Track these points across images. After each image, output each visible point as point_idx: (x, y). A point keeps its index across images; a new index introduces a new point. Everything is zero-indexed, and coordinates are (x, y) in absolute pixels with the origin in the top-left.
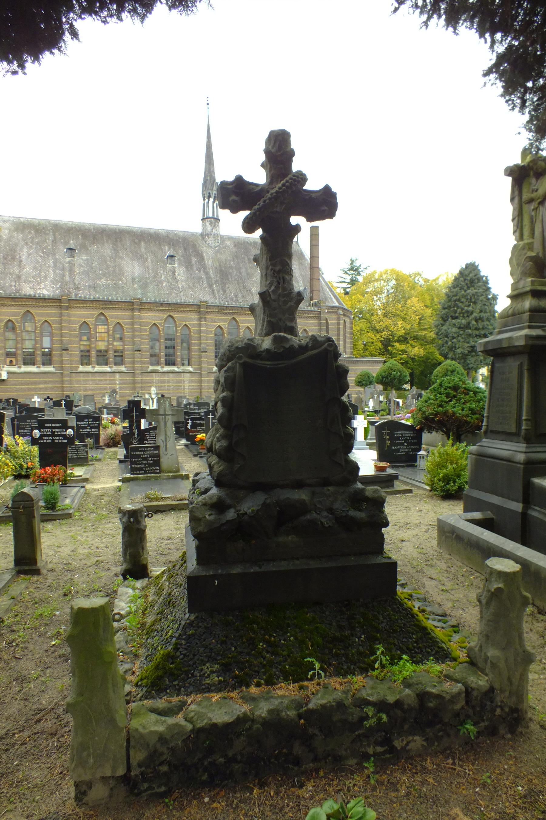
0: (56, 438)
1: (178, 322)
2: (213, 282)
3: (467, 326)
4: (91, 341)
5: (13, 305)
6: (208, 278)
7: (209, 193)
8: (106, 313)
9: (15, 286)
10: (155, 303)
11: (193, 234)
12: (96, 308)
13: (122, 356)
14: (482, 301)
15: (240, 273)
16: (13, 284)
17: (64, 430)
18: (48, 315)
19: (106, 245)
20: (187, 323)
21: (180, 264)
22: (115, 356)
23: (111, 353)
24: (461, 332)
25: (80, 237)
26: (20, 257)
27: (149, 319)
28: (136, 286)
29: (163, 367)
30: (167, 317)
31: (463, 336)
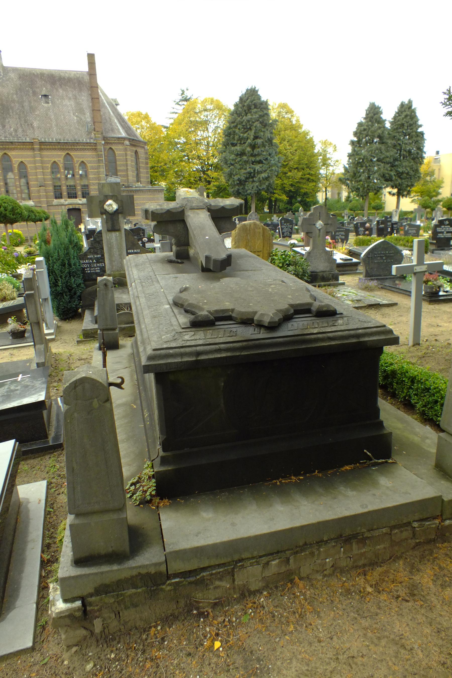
3: (242, 154)
14: (256, 127)
15: (23, 107)
18: (22, 156)
30: (65, 156)
31: (240, 163)
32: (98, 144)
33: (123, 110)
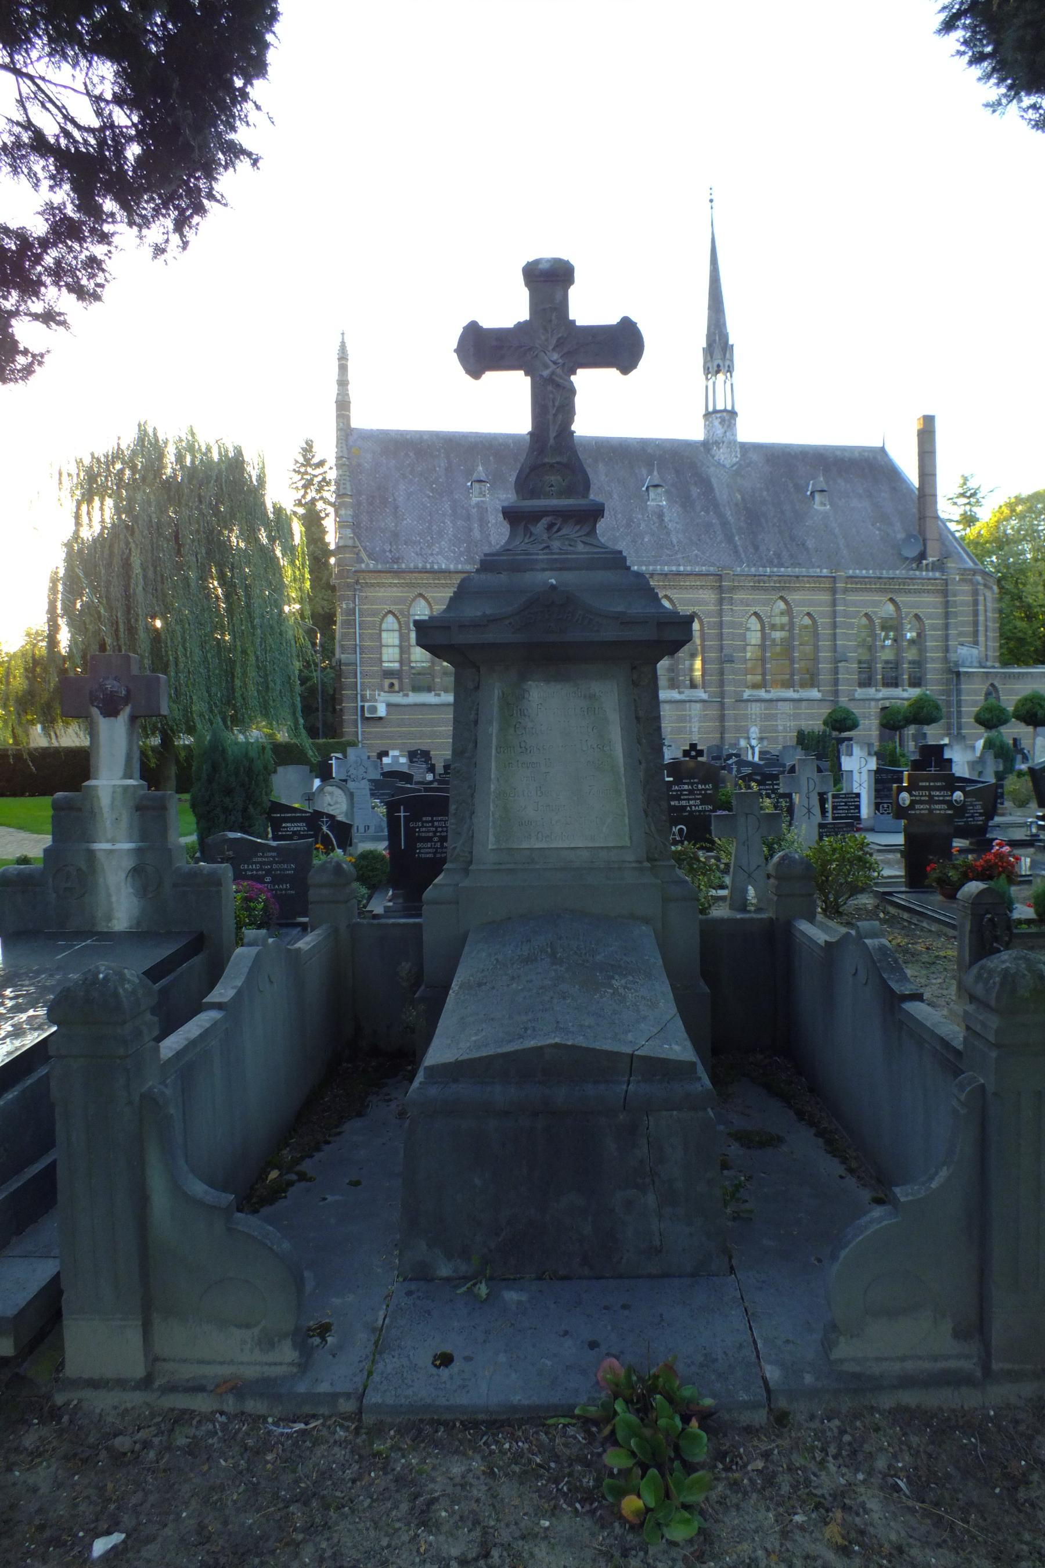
0: (937, 807)
2: (734, 531)
5: (395, 585)
9: (391, 551)
16: (387, 547)
17: (949, 793)
25: (491, 458)
26: (395, 500)
32: (949, 582)
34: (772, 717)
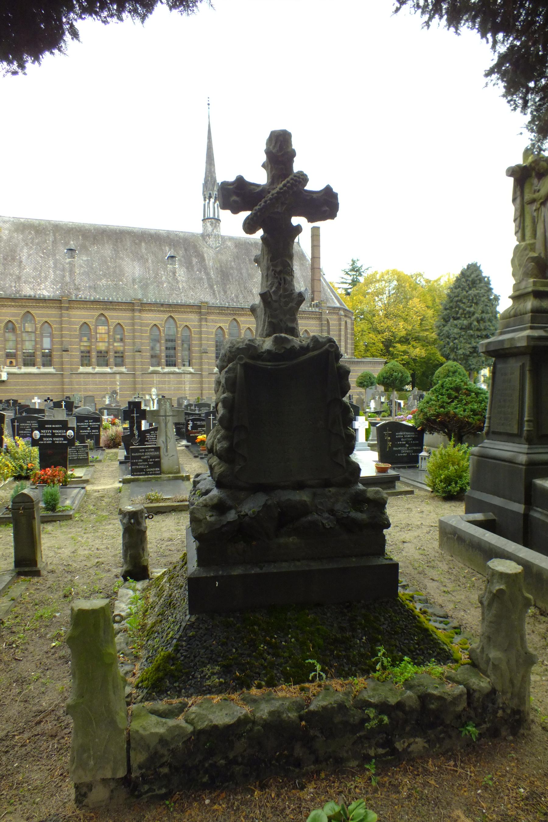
0: (56, 439)
1: (178, 323)
2: (214, 283)
3: (469, 327)
4: (91, 342)
5: (13, 306)
6: (209, 279)
7: (210, 194)
8: (107, 313)
9: (15, 287)
10: (155, 304)
11: (193, 235)
12: (96, 309)
13: (122, 357)
14: (483, 301)
15: (241, 274)
16: (13, 284)
17: (64, 431)
18: (48, 316)
19: (106, 245)
20: (187, 324)
21: (181, 265)
22: (116, 357)
23: (111, 354)
24: (463, 333)
25: (80, 237)
26: (20, 258)
27: (150, 320)
28: (136, 286)
29: (164, 368)
31: (465, 337)
33: (514, 282)
34: (180, 383)
